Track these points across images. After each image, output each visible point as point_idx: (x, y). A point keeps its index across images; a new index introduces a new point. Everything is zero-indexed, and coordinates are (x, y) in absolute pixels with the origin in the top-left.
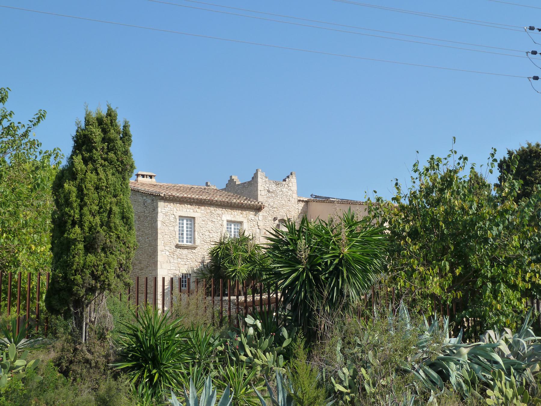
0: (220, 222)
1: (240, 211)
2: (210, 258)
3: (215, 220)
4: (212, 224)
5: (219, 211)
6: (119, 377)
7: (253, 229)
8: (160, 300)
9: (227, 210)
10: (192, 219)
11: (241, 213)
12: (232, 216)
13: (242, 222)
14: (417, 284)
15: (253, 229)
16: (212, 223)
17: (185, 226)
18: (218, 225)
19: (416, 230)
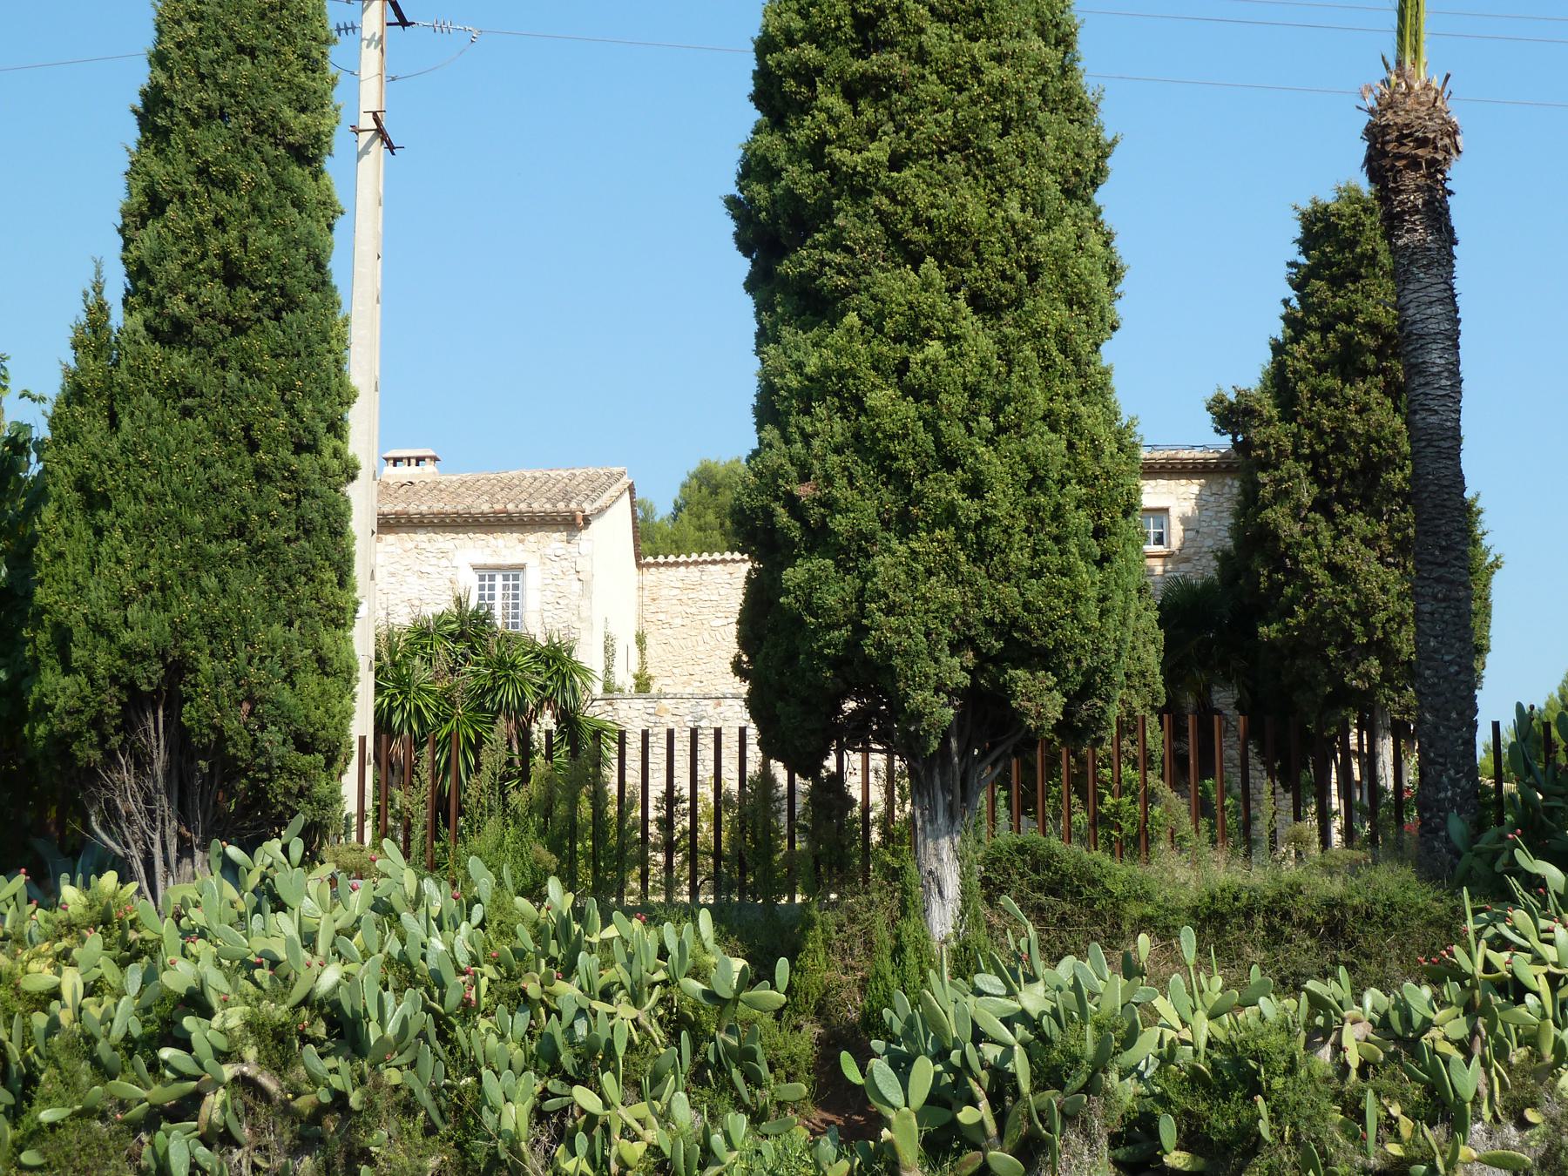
0: (448, 574)
1: (515, 535)
2: (79, 877)
3: (429, 569)
4: (421, 581)
5: (444, 541)
6: (906, 236)
7: (559, 582)
8: (1337, 812)
9: (471, 535)
10: (515, 571)
11: (521, 541)
12: (488, 551)
13: (521, 567)
14: (1334, 305)
15: (559, 582)
16: (420, 577)
17: (498, 592)
18: (440, 582)
19: (574, 519)
